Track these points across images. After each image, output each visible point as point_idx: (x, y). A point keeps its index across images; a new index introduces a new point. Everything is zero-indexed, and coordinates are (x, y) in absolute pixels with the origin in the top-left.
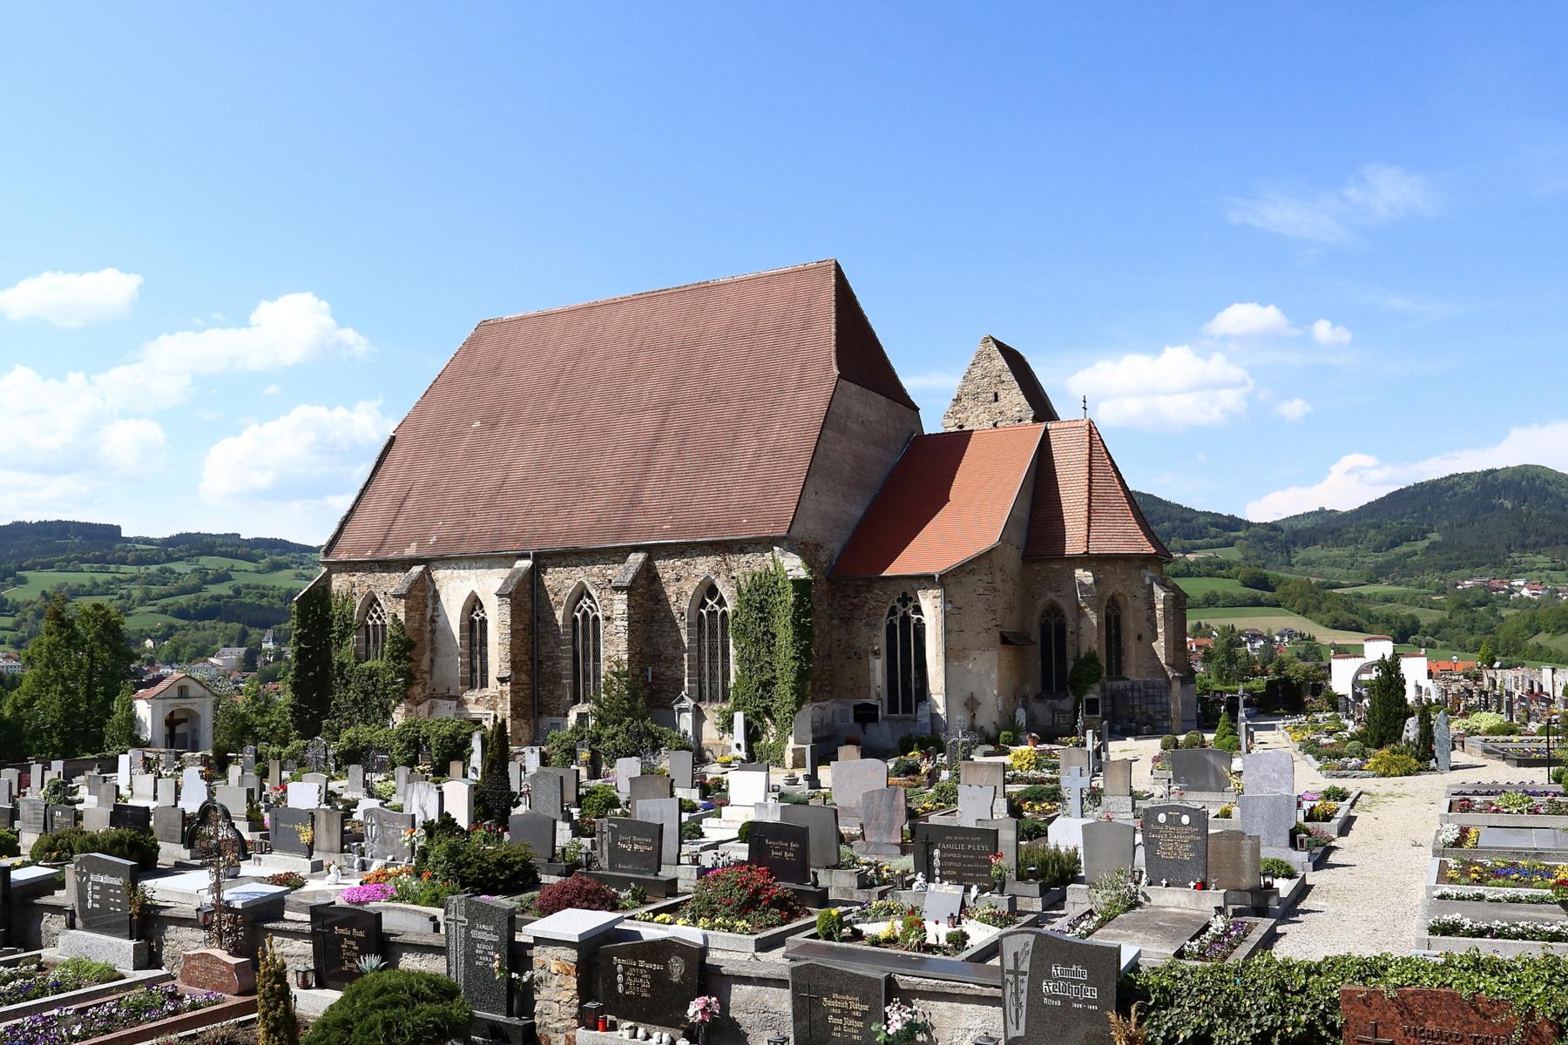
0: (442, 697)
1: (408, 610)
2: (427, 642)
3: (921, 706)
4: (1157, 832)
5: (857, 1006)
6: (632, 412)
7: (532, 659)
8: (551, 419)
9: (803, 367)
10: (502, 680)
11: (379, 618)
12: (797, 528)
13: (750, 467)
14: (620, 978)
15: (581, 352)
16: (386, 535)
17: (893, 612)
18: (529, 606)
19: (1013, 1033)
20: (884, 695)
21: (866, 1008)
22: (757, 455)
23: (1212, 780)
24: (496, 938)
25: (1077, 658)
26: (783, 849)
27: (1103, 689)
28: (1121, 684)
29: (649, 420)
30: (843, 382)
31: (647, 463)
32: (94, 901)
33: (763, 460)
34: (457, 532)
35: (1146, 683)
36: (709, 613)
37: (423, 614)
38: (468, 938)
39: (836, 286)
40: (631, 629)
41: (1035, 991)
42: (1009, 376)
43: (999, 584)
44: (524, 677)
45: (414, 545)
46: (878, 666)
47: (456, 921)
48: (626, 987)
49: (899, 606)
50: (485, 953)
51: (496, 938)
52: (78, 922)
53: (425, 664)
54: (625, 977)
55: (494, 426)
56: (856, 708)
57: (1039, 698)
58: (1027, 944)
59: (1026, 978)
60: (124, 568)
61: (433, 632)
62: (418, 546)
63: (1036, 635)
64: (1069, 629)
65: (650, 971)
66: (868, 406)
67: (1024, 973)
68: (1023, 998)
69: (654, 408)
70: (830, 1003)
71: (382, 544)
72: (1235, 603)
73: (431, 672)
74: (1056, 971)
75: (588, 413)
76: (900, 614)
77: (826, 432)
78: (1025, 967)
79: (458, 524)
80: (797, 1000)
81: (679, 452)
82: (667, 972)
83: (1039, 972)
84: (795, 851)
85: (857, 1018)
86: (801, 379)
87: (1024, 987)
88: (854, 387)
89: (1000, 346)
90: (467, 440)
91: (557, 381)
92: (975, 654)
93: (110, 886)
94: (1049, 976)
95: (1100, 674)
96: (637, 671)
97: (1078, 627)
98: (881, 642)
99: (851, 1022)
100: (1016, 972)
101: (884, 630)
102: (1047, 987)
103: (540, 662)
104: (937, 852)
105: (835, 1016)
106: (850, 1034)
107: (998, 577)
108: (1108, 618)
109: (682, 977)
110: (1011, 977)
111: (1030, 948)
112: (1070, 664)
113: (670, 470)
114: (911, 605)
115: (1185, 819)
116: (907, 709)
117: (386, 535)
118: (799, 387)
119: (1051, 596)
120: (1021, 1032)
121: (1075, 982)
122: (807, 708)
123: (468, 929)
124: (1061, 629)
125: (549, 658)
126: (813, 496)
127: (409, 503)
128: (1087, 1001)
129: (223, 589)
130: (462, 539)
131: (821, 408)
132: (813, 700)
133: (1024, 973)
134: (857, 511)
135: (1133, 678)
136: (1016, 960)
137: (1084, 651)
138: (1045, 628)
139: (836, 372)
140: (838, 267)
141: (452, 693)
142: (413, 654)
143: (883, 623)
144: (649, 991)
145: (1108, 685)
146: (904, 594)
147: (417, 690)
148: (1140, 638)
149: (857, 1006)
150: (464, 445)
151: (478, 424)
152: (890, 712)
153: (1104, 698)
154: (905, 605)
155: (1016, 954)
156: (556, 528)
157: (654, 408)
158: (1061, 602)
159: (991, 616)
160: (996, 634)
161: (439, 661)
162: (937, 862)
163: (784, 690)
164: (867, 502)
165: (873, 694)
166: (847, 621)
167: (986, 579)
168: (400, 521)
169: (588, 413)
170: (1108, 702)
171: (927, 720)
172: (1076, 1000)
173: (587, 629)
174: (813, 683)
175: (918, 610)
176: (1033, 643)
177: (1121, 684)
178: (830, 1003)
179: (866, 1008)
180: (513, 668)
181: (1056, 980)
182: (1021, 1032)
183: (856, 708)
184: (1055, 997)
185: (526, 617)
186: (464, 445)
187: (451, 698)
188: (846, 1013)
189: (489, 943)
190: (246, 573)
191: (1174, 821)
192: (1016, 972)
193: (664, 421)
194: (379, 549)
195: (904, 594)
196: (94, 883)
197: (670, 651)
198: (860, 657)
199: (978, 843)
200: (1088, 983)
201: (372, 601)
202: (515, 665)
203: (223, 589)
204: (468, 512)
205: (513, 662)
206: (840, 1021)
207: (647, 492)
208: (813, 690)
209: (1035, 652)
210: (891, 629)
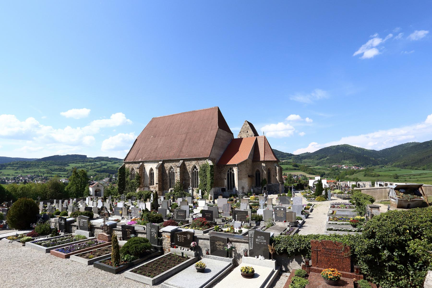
9: (212, 126)
10: (157, 184)
12: (211, 156)
17: (228, 171)
19: (251, 249)
20: (227, 187)
22: (204, 142)
23: (287, 202)
29: (184, 136)
31: (183, 144)
34: (149, 156)
38: (150, 231)
40: (180, 174)
41: (254, 241)
42: (250, 128)
43: (248, 166)
46: (226, 181)
52: (79, 228)
53: (142, 181)
55: (155, 137)
57: (255, 187)
60: (87, 163)
63: (255, 176)
66: (224, 133)
68: (252, 242)
72: (291, 170)
74: (258, 237)
78: (253, 236)
82: (187, 237)
89: (248, 122)
94: (257, 238)
98: (226, 177)
100: (251, 237)
102: (257, 240)
107: (248, 165)
112: (261, 181)
113: (188, 145)
115: (282, 209)
116: (231, 189)
118: (211, 130)
120: (252, 248)
122: (213, 189)
123: (150, 230)
124: (259, 174)
127: (140, 151)
128: (264, 243)
129: (106, 167)
131: (215, 134)
138: (256, 174)
147: (141, 186)
156: (167, 156)
160: (247, 175)
162: (236, 217)
163: (208, 185)
166: (220, 173)
168: (138, 155)
173: (172, 174)
175: (233, 171)
182: (252, 248)
188: (220, 245)
190: (110, 164)
191: (280, 210)
192: (251, 237)
197: (188, 178)
198: (222, 179)
202: (159, 181)
203: (106, 167)
207: (183, 149)
209: (254, 178)
210: (228, 174)
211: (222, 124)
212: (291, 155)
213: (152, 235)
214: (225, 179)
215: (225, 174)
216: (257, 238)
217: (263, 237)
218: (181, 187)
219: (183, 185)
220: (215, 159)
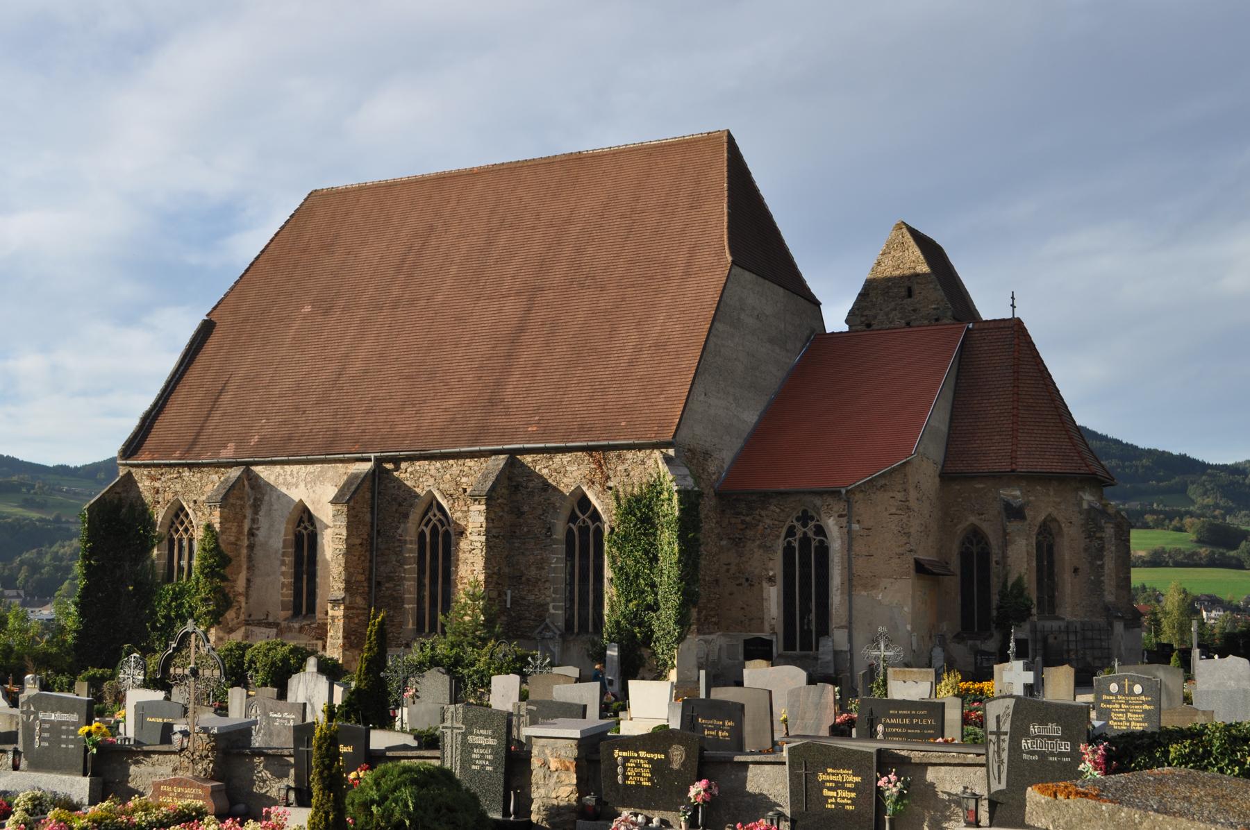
0: (259, 624)
1: (224, 520)
2: (244, 560)
3: (823, 641)
4: (1109, 702)
5: (850, 779)
6: (490, 298)
7: (369, 580)
8: (395, 305)
9: (692, 252)
11: (186, 530)
12: (684, 432)
13: (631, 363)
14: (620, 770)
15: (432, 228)
16: (198, 434)
17: (791, 532)
18: (368, 518)
19: (995, 787)
20: (780, 629)
21: (858, 779)
22: (638, 350)
24: (493, 742)
25: (1003, 595)
26: (717, 728)
27: (1034, 630)
28: (1055, 624)
29: (512, 308)
30: (737, 270)
31: (509, 356)
32: (42, 739)
33: (645, 355)
34: (284, 431)
35: (1083, 624)
36: (580, 528)
37: (240, 527)
38: (464, 742)
39: (729, 160)
40: (490, 546)
41: (1015, 748)
43: (913, 504)
44: (359, 600)
45: (231, 445)
46: (773, 596)
47: (452, 728)
48: (626, 778)
49: (798, 525)
50: (482, 757)
51: (493, 742)
52: (23, 763)
53: (241, 584)
54: (625, 768)
55: (327, 311)
56: (747, 642)
57: (959, 638)
58: (1007, 708)
59: (1007, 738)
61: (251, 547)
62: (237, 448)
63: (955, 564)
64: (994, 558)
65: (650, 761)
66: (761, 297)
67: (1006, 733)
68: (1005, 755)
69: (518, 294)
70: (825, 777)
71: (194, 443)
72: (1189, 561)
73: (247, 596)
74: (1034, 729)
75: (440, 298)
76: (799, 535)
77: (717, 324)
78: (1006, 727)
79: (285, 422)
80: (794, 777)
81: (547, 344)
82: (668, 761)
83: (1019, 731)
84: (731, 730)
85: (850, 790)
86: (689, 264)
87: (1005, 745)
88: (748, 275)
89: (915, 234)
90: (296, 326)
91: (403, 261)
92: (885, 582)
93: (62, 723)
94: (1027, 734)
95: (1029, 609)
96: (494, 594)
97: (1005, 557)
98: (776, 567)
99: (846, 794)
100: (998, 733)
101: (780, 553)
102: (1026, 744)
103: (379, 583)
104: (880, 728)
105: (830, 789)
106: (843, 805)
107: (913, 494)
108: (1039, 546)
109: (683, 764)
110: (993, 738)
111: (1010, 711)
112: (995, 599)
113: (537, 365)
114: (811, 524)
116: (806, 645)
117: (198, 434)
118: (687, 274)
119: (973, 519)
120: (1003, 786)
121: (1050, 738)
122: (693, 640)
123: (464, 735)
124: (985, 557)
125: (390, 579)
126: (702, 398)
127: (226, 398)
128: (1061, 754)
130: (290, 438)
131: (711, 298)
132: (699, 632)
133: (1006, 733)
134: (750, 417)
135: (1068, 618)
136: (998, 722)
137: (1011, 580)
138: (966, 557)
139: (730, 259)
140: (731, 140)
141: (271, 619)
142: (227, 572)
143: (780, 544)
144: (650, 779)
145: (1040, 625)
146: (805, 512)
147: (230, 615)
148: (1076, 570)
149: (850, 779)
150: (292, 332)
151: (308, 309)
152: (786, 648)
153: (1035, 641)
154: (805, 525)
155: (998, 717)
156: (401, 429)
157: (518, 294)
158: (986, 527)
159: (904, 539)
160: (910, 559)
161: (258, 581)
163: (665, 620)
164: (761, 408)
165: (767, 627)
166: (738, 542)
167: (899, 496)
168: (216, 417)
169: (440, 298)
170: (1039, 646)
171: (830, 658)
172: (1052, 754)
173: (441, 541)
174: (699, 612)
175: (820, 531)
176: (953, 574)
177: (1055, 624)
178: (825, 777)
179: (858, 779)
180: (346, 590)
181: (1033, 738)
182: (1003, 786)
183: (747, 642)
184: (1033, 753)
185: (364, 531)
186: (292, 332)
187: (269, 625)
188: (839, 786)
189: (486, 747)
192: (998, 733)
193: (529, 310)
194: (188, 451)
195: (805, 512)
196: (43, 721)
197: (533, 572)
198: (751, 582)
199: (922, 717)
200: (1062, 738)
201: (178, 512)
202: (349, 587)
204: (297, 409)
205: (348, 582)
206: (833, 794)
207: (509, 390)
208: (698, 620)
209: (953, 584)
210: (788, 552)
211: (756, 239)
212: (1186, 465)
213: (473, 762)
214: (771, 580)
215: (767, 548)
216: (1027, 734)
217: (1054, 729)
218: (489, 623)
219: (504, 610)
220: (707, 454)
